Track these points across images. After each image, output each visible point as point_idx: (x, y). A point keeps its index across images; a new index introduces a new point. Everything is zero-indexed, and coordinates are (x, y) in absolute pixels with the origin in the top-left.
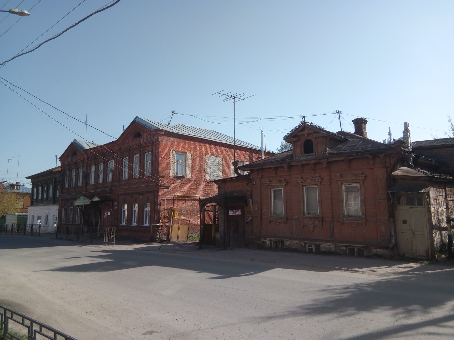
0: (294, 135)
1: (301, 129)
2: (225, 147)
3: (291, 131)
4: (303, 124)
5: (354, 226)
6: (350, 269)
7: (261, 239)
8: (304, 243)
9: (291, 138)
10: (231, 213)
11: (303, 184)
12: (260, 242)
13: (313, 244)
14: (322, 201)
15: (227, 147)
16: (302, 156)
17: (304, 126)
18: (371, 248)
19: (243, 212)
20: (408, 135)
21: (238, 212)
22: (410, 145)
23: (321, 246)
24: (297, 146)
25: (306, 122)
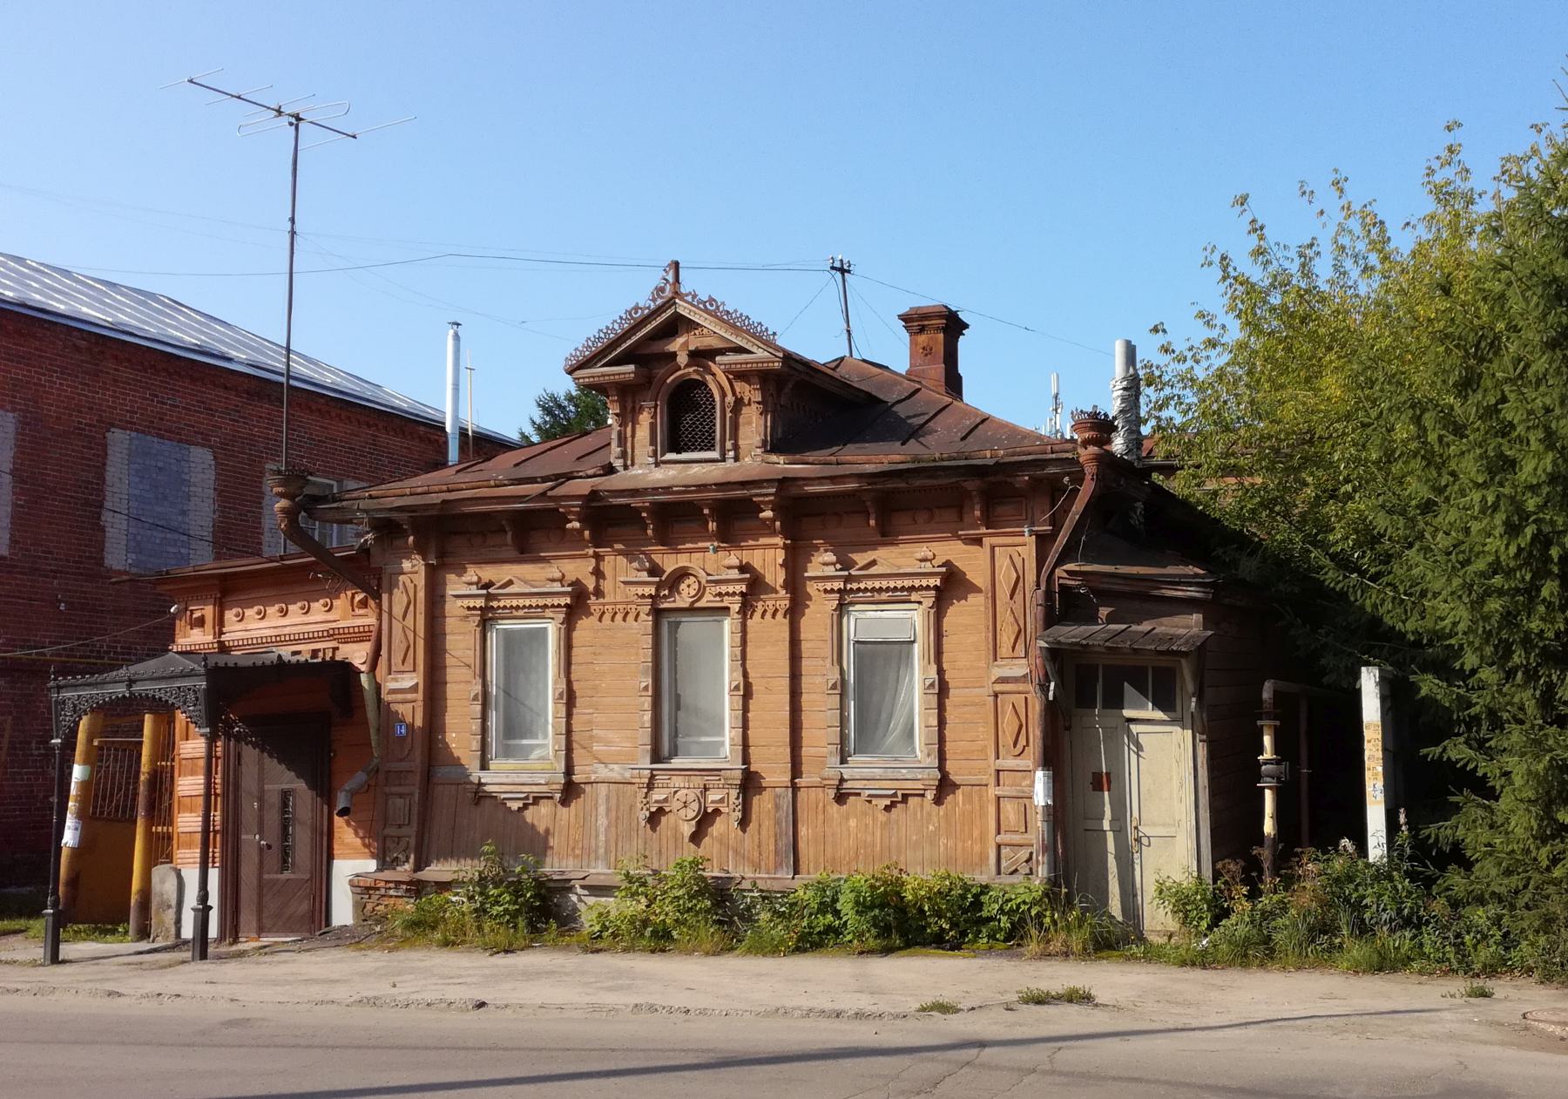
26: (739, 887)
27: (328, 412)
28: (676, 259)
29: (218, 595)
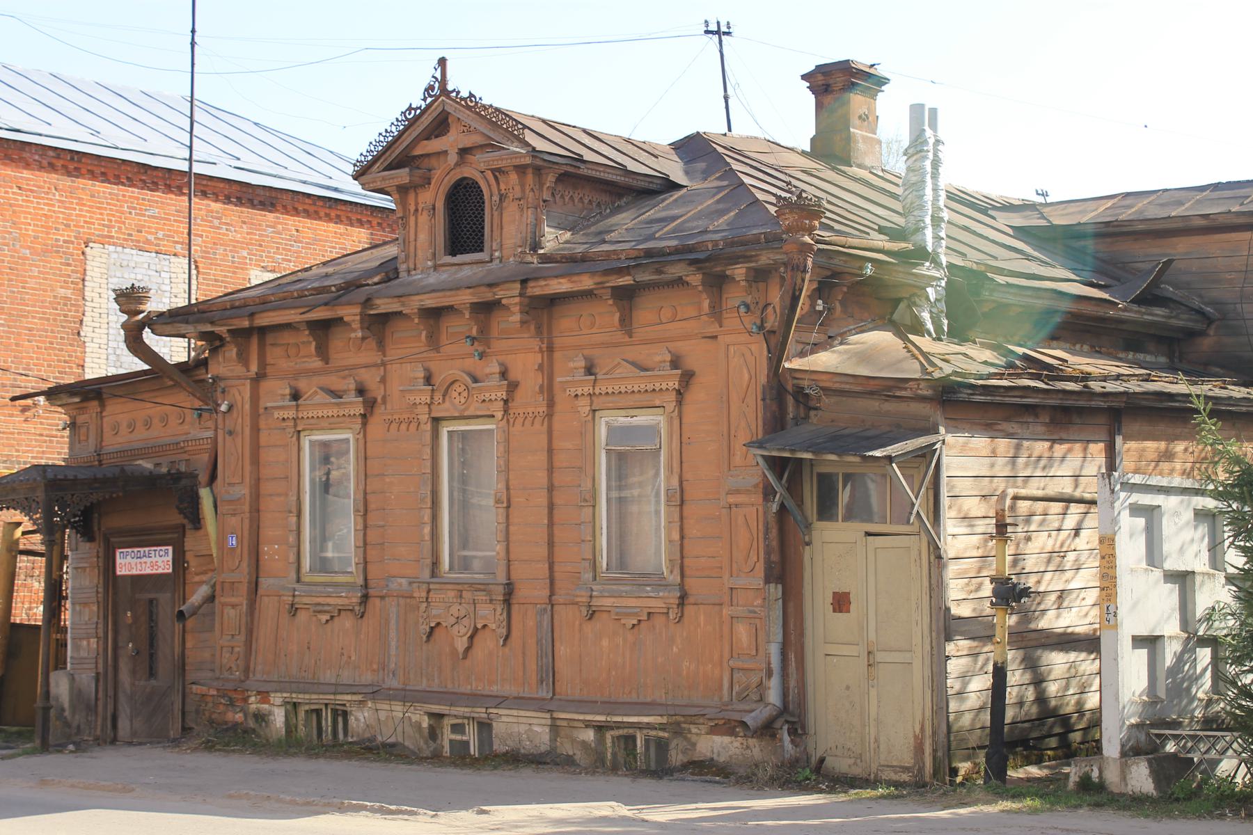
0: (397, 152)
1: (426, 120)
2: (216, 201)
3: (386, 131)
4: (437, 98)
5: (634, 625)
6: (391, 807)
7: (246, 700)
8: (432, 715)
9: (384, 170)
10: (130, 563)
11: (434, 415)
12: (239, 717)
13: (468, 718)
14: (509, 501)
15: (228, 200)
16: (436, 267)
17: (440, 109)
18: (694, 730)
19: (179, 560)
20: (922, 168)
21: (158, 561)
22: (928, 220)
23: (498, 728)
24: (416, 210)
25: (450, 88)
26: (1206, 756)
27: (316, 212)
28: (441, 56)
29: (99, 410)
